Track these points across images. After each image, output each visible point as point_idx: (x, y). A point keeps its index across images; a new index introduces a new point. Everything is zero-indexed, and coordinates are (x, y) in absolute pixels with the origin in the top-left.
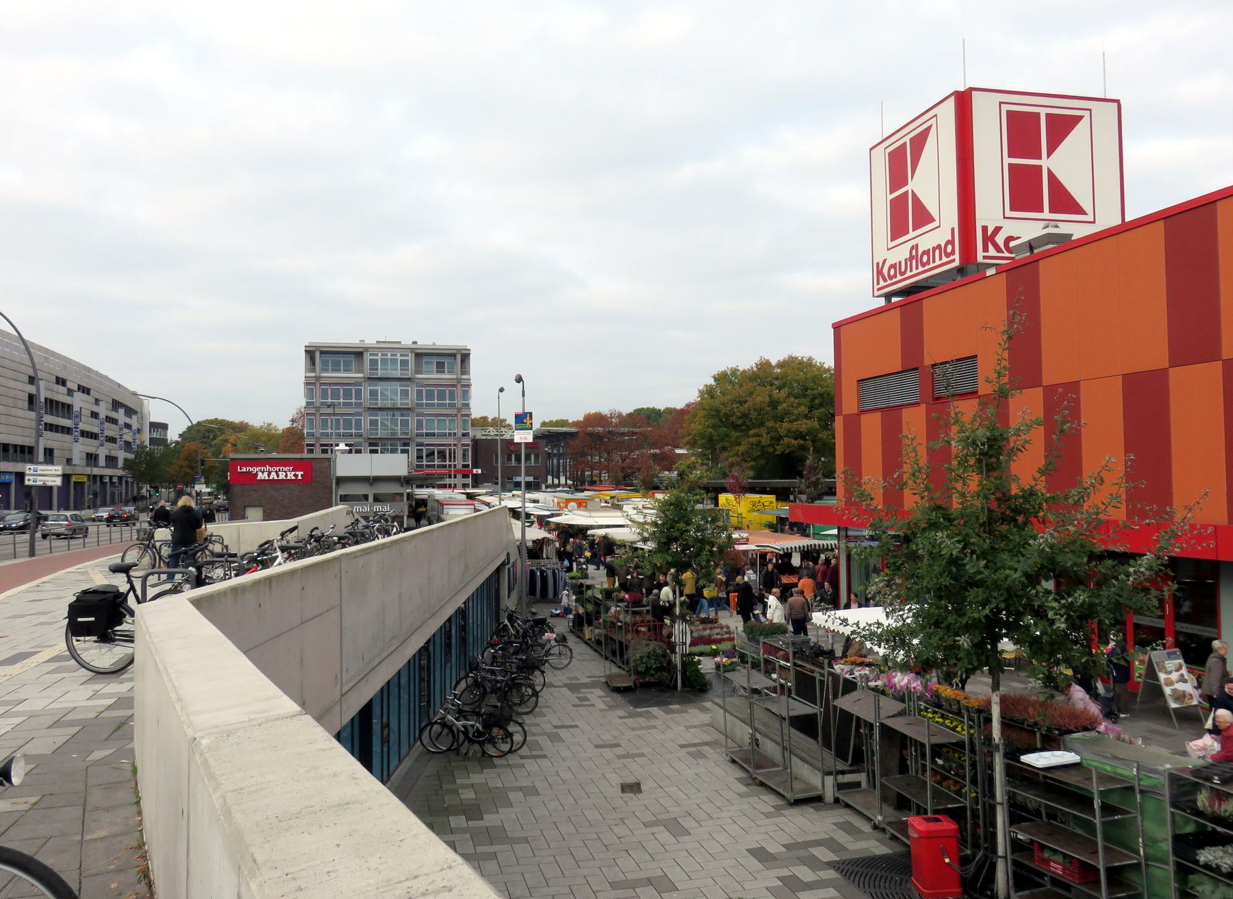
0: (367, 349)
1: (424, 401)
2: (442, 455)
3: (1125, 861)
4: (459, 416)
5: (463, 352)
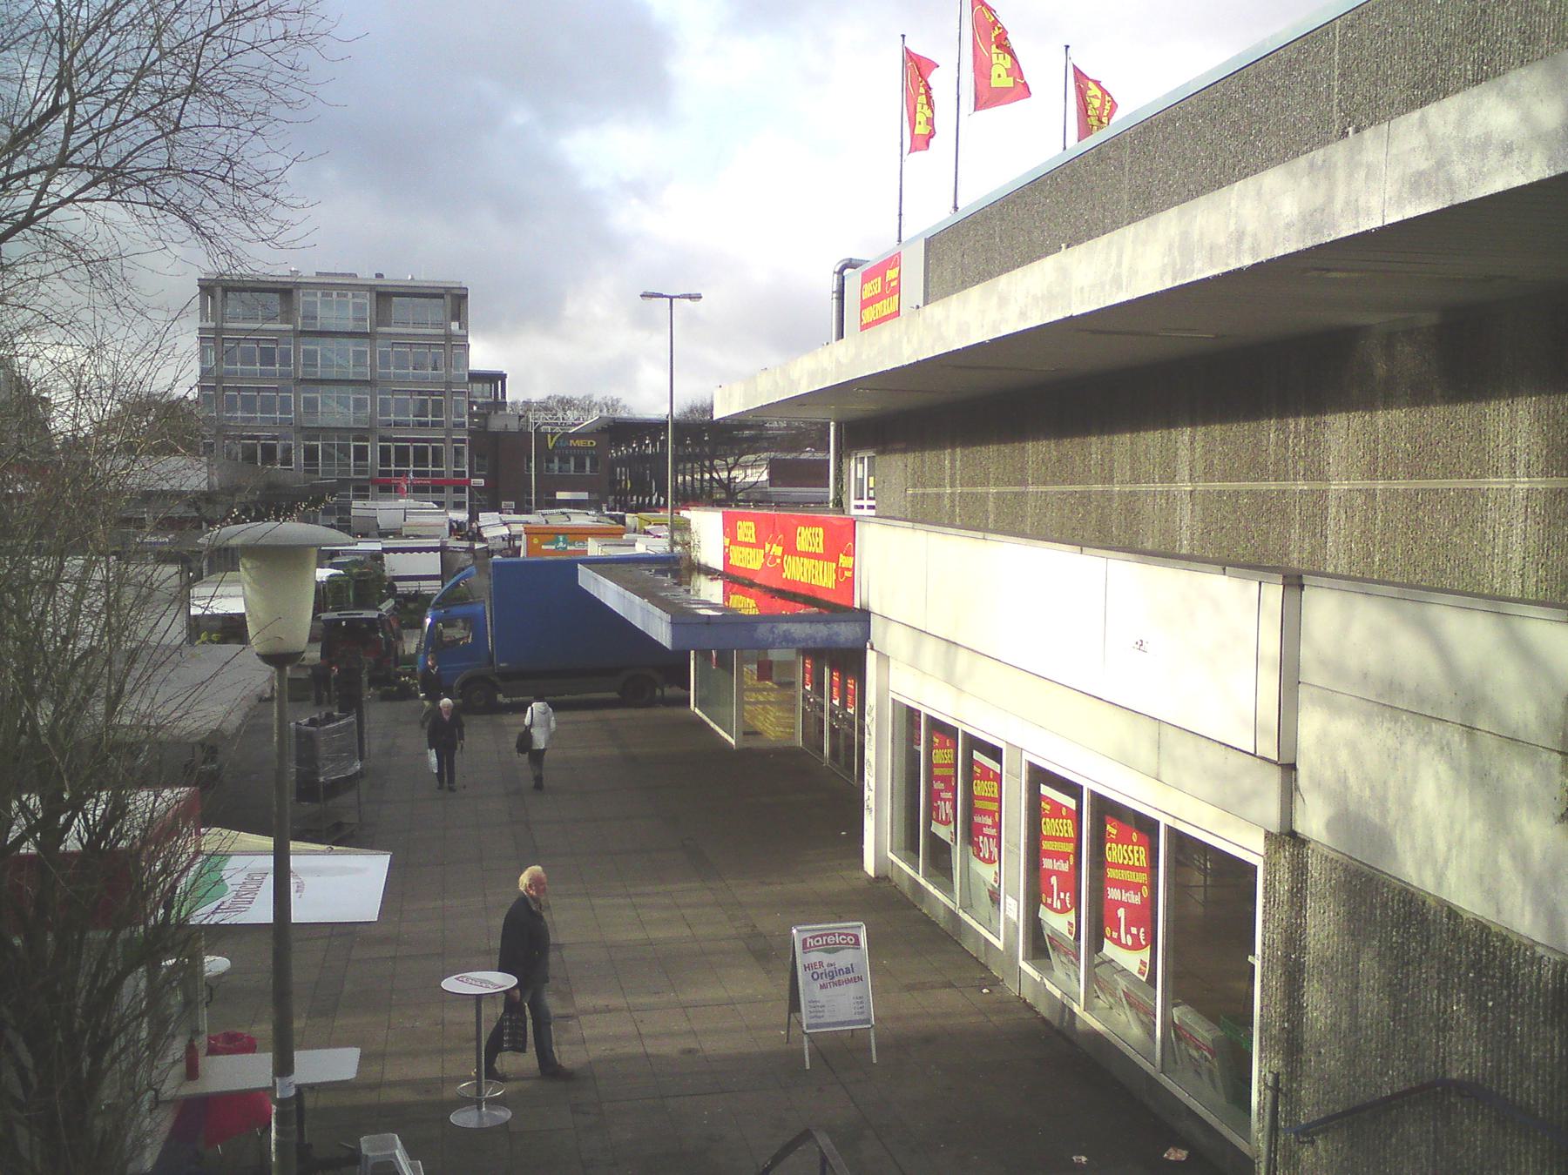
0: (298, 285)
1: (393, 468)
2: (421, 456)
3: (277, 1123)
4: (449, 441)
5: (456, 292)
